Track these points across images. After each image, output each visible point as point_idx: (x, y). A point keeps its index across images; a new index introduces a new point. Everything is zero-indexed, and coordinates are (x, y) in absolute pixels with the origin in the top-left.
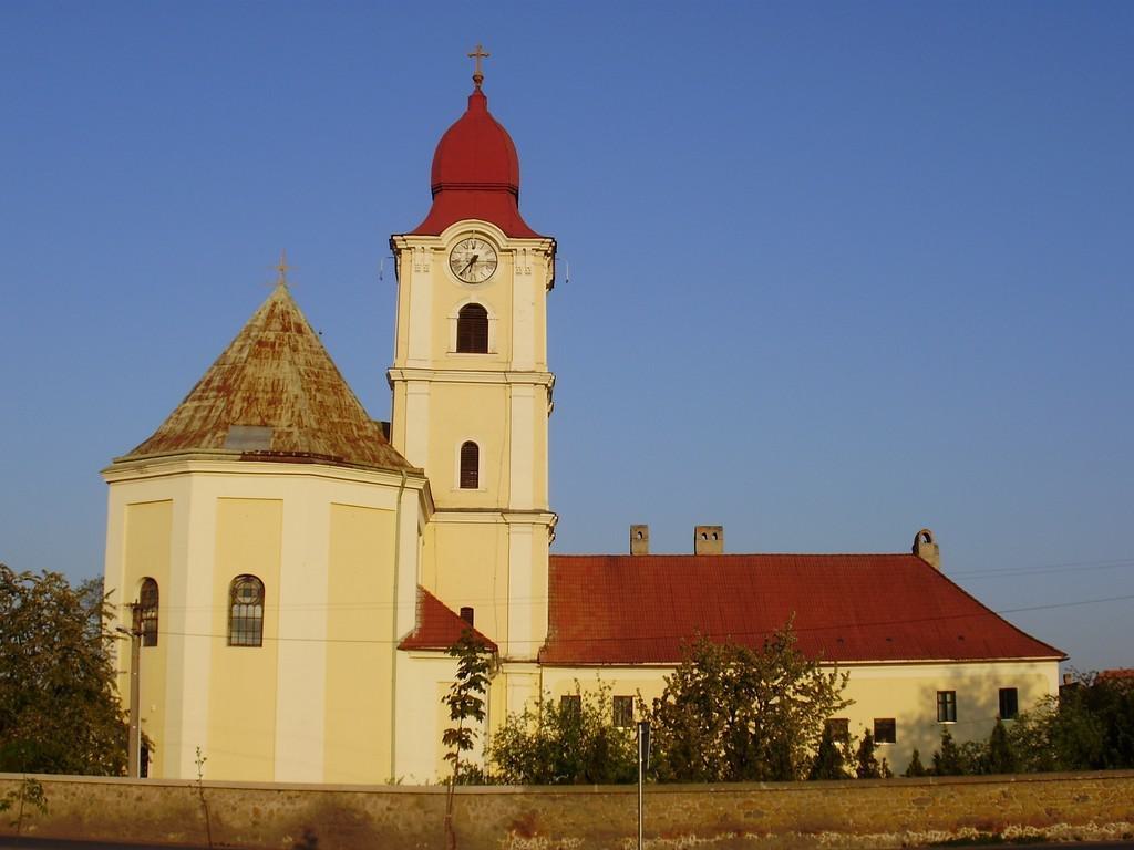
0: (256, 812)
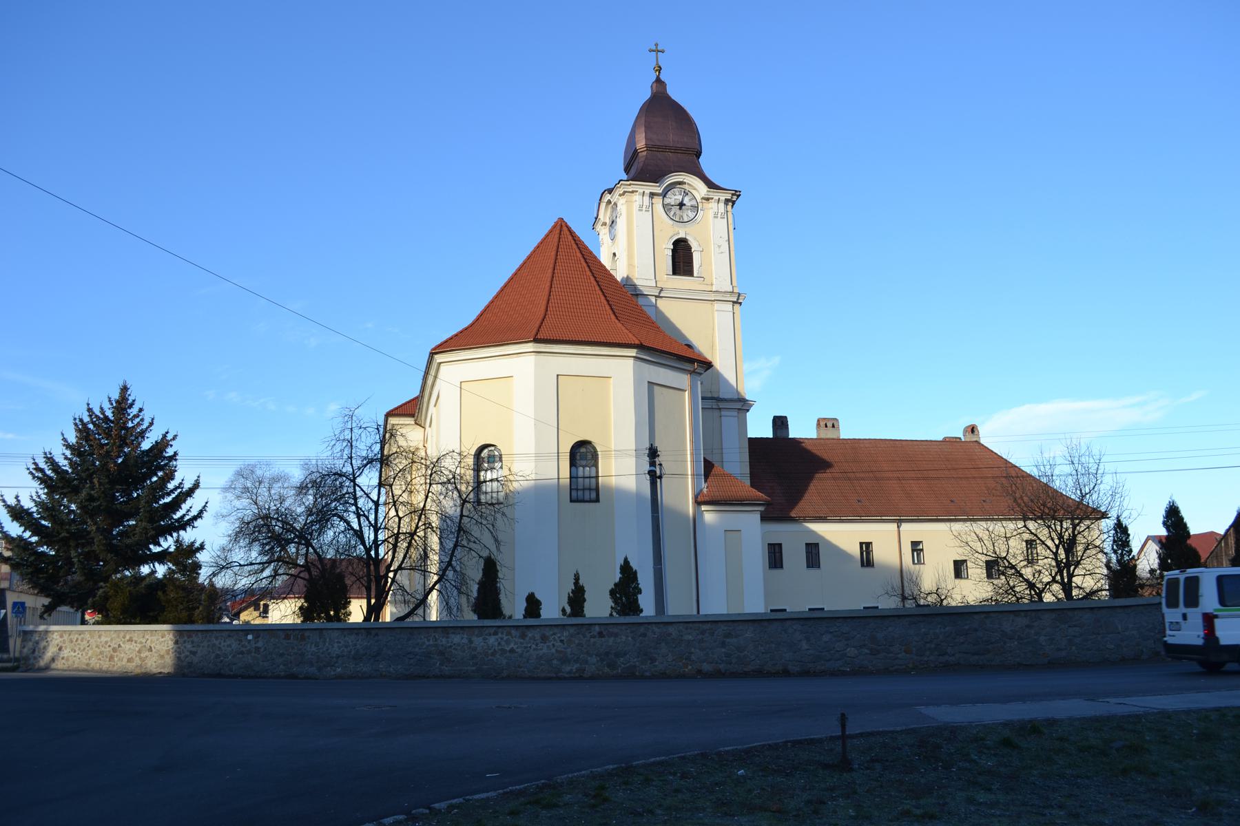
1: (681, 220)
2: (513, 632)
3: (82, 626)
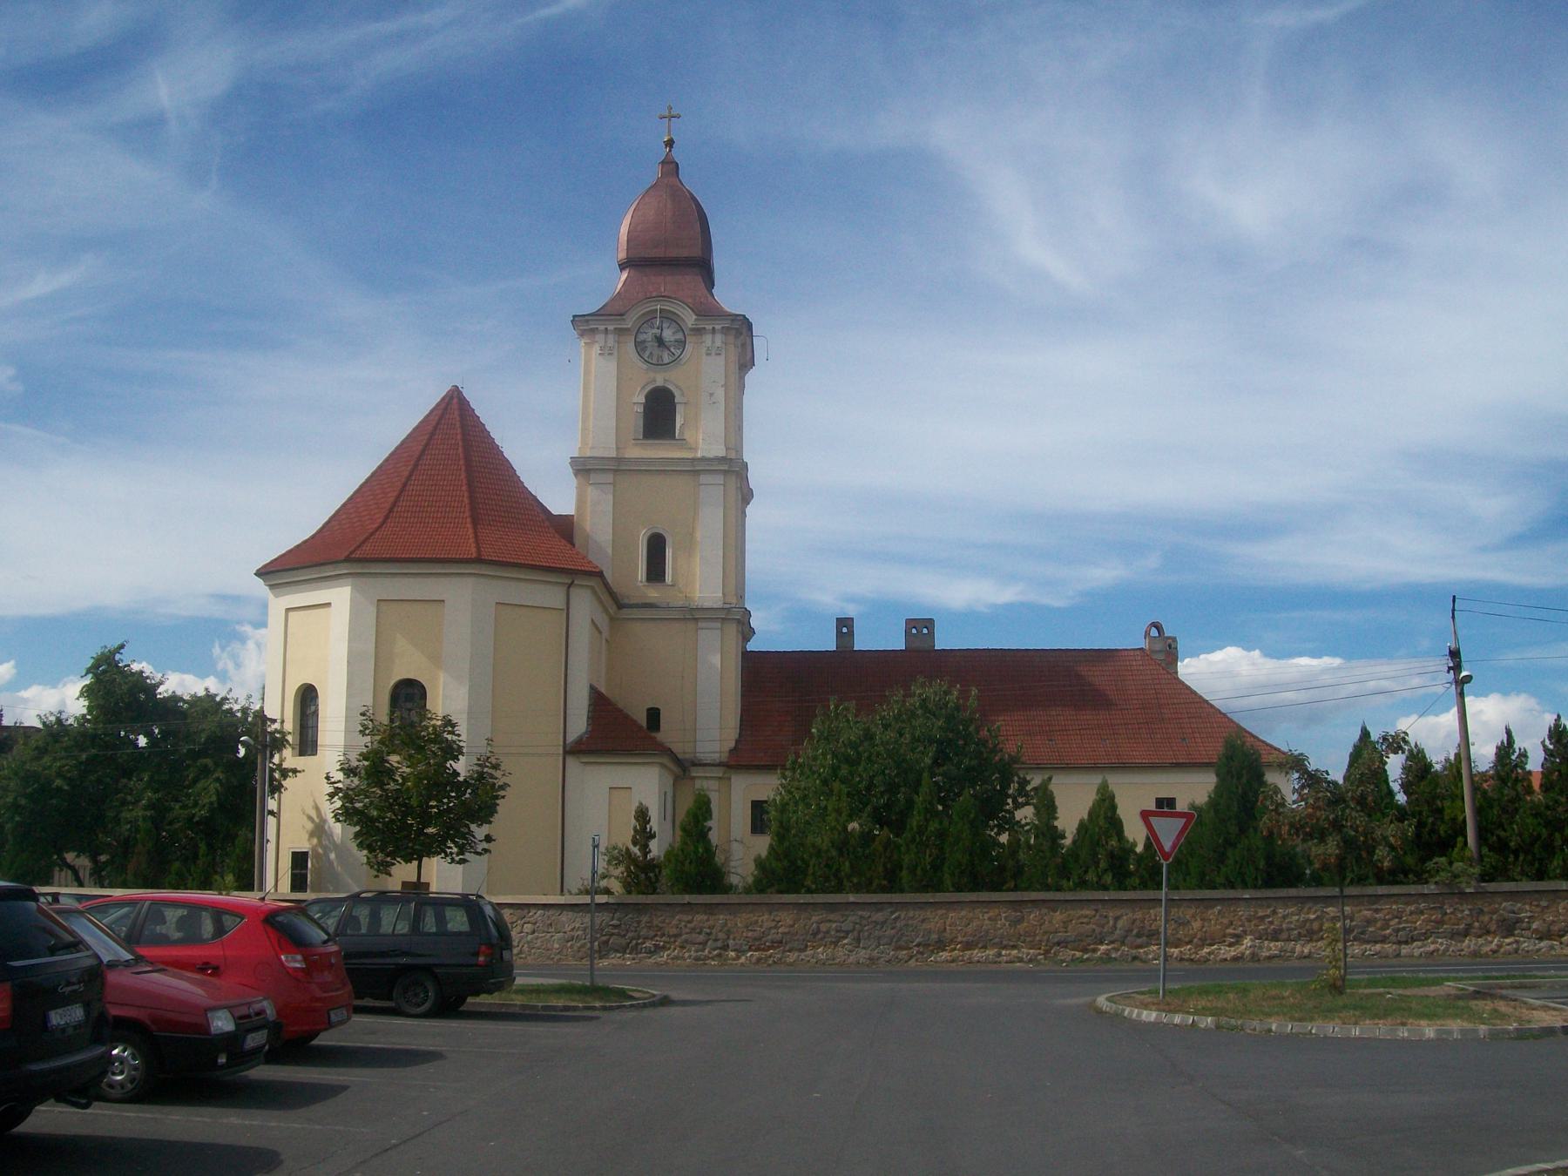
1: (660, 362)
3: (81, 888)
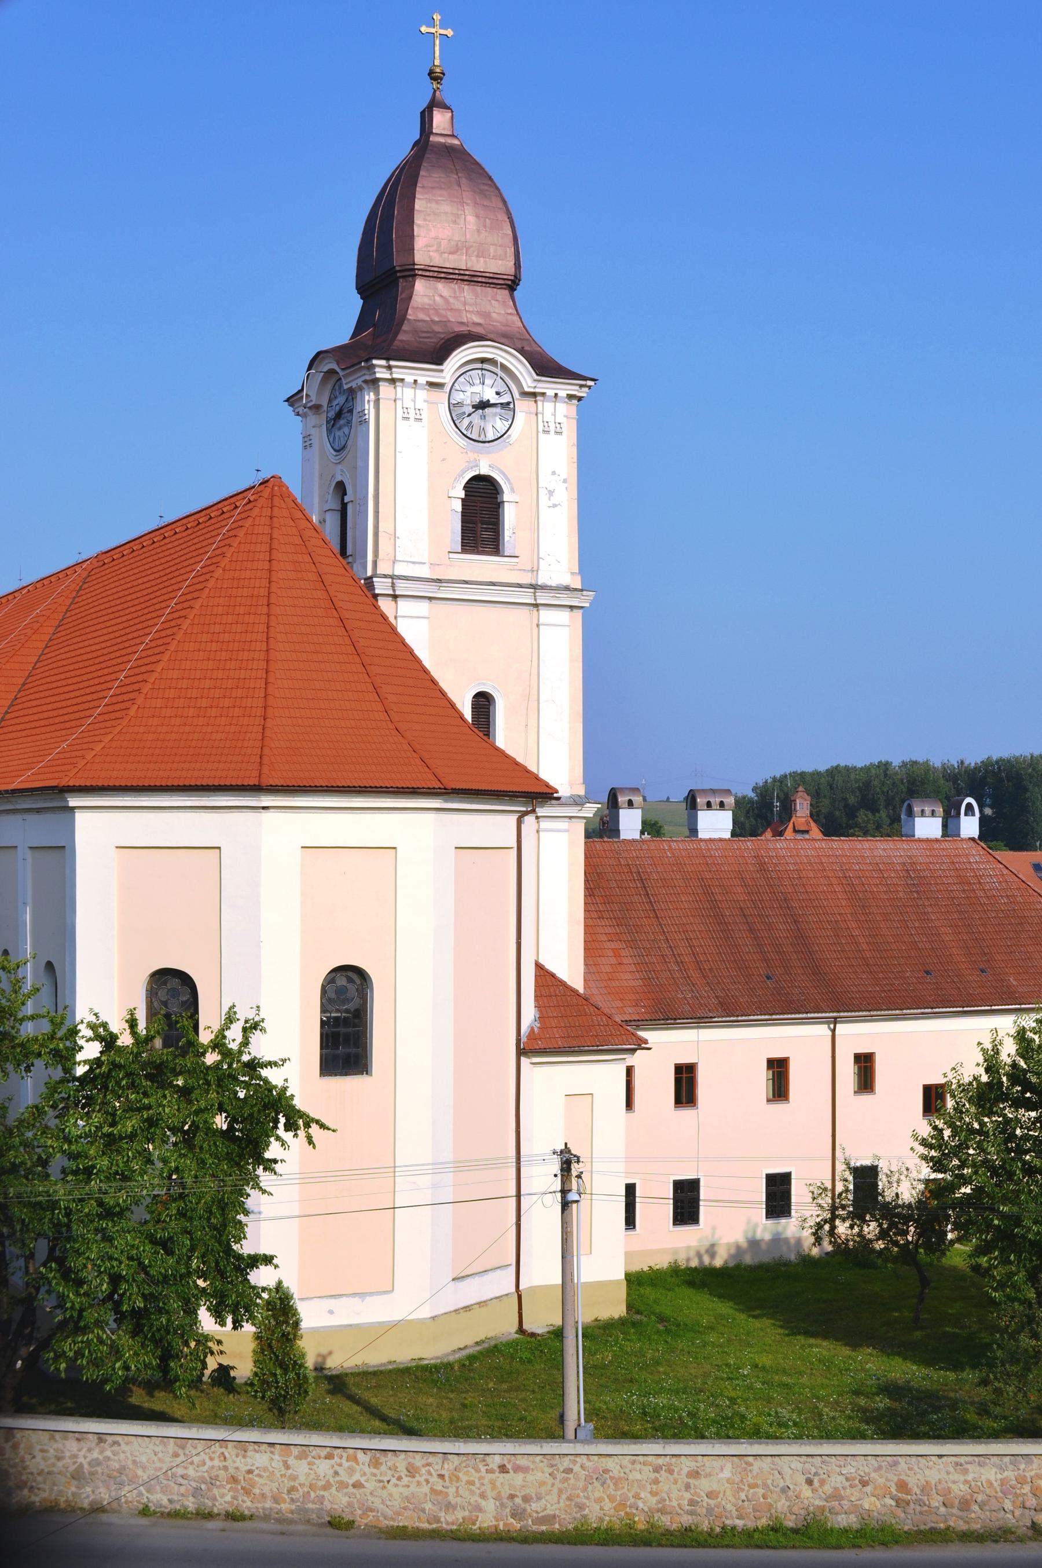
0: (902, 1486)
1: (482, 438)
2: (360, 1455)
